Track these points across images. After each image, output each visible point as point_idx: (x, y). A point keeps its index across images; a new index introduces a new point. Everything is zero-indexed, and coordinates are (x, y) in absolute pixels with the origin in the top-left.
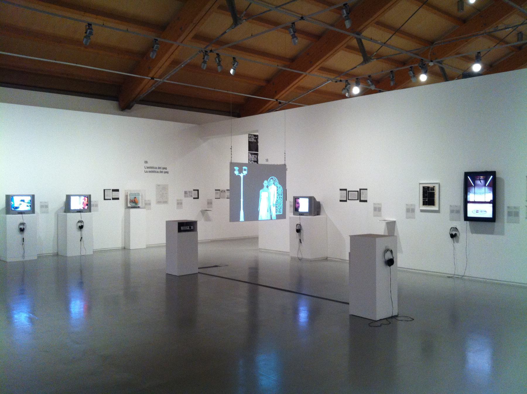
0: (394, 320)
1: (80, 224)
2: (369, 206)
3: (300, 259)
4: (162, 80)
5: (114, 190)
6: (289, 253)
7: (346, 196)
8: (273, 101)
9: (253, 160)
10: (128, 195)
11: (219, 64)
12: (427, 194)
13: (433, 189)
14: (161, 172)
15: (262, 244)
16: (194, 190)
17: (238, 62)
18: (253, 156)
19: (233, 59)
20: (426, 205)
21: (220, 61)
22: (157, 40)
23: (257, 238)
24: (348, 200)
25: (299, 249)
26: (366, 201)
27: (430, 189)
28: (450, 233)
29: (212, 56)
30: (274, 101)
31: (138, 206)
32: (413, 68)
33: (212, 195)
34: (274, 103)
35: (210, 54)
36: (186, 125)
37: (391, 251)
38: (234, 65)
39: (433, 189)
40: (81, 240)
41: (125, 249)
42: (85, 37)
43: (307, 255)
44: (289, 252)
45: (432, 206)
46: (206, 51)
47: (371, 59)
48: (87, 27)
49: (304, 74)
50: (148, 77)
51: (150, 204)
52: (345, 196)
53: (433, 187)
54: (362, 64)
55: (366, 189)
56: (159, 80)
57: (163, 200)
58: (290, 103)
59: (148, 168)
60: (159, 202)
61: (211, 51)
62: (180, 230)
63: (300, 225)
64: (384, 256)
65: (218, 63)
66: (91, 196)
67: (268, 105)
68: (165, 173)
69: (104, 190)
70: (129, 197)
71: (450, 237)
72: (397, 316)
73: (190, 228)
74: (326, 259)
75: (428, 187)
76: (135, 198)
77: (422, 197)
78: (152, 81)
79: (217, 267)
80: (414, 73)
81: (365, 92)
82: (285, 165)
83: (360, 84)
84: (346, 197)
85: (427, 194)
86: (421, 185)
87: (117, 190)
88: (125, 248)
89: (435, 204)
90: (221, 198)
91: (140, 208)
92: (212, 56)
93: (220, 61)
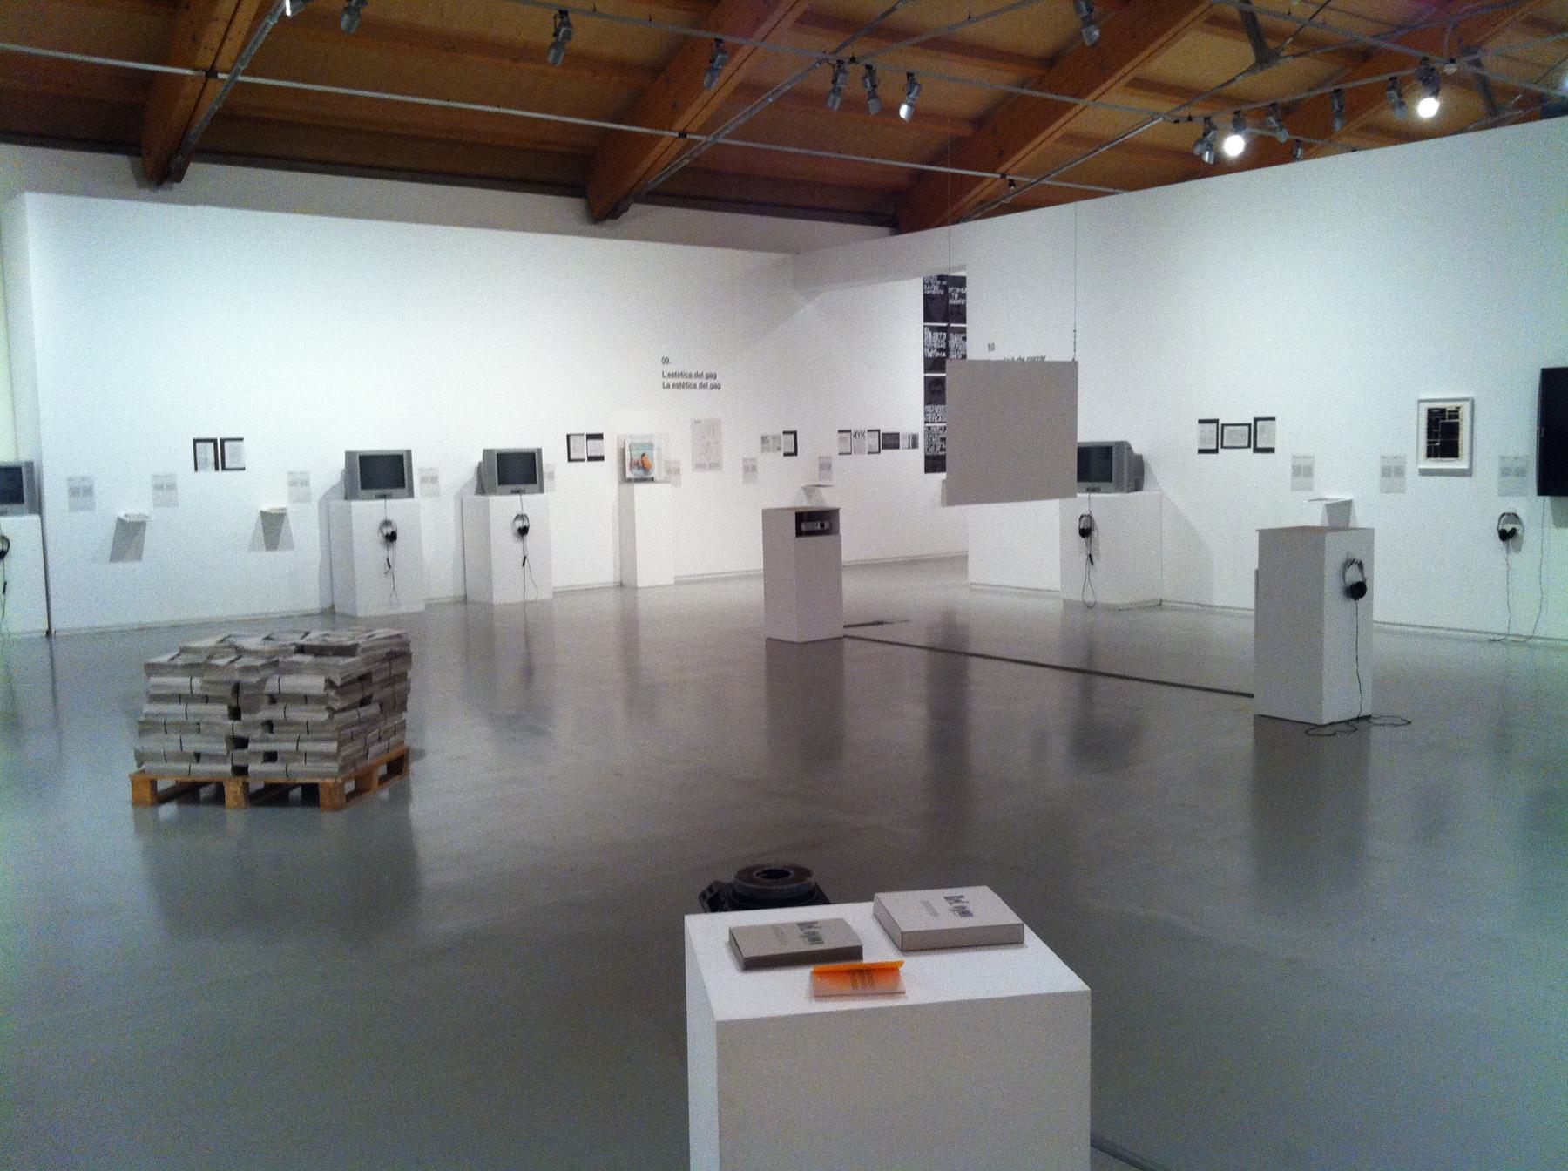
0: (1362, 724)
1: (519, 524)
2: (1278, 464)
3: (1090, 607)
4: (710, 138)
5: (590, 437)
6: (1058, 592)
7: (1215, 438)
8: (992, 178)
9: (935, 345)
10: (627, 448)
11: (873, 95)
12: (1438, 428)
13: (1455, 414)
14: (703, 386)
15: (978, 572)
16: (784, 433)
17: (919, 85)
18: (937, 334)
19: (908, 78)
20: (1436, 456)
21: (874, 86)
22: (721, 41)
23: (966, 557)
24: (1220, 449)
25: (1087, 579)
26: (1271, 450)
27: (1447, 413)
28: (1498, 528)
29: (856, 71)
30: (996, 179)
31: (651, 476)
32: (1398, 81)
33: (830, 444)
34: (996, 184)
35: (849, 67)
36: (775, 256)
37: (1360, 565)
38: (909, 93)
39: (1455, 414)
40: (524, 564)
41: (624, 586)
42: (554, 45)
43: (1109, 592)
44: (1059, 589)
45: (1453, 459)
46: (840, 62)
47: (1278, 55)
48: (559, 20)
49: (1082, 103)
50: (670, 130)
51: (677, 471)
52: (1213, 439)
53: (1454, 409)
54: (1251, 70)
55: (1273, 419)
56: (703, 138)
57: (708, 461)
58: (1045, 181)
59: (671, 375)
60: (699, 466)
61: (853, 60)
62: (799, 533)
63: (1090, 517)
64: (1344, 576)
65: (869, 92)
66: (543, 452)
67: (977, 190)
68: (712, 388)
69: (568, 436)
70: (627, 454)
71: (1498, 536)
72: (1368, 718)
73: (822, 525)
74: (1159, 605)
75: (1443, 411)
76: (643, 455)
77: (1426, 435)
78: (682, 140)
79: (879, 626)
80: (1400, 95)
81: (1262, 156)
82: (1074, 364)
83: (1244, 129)
84: (1215, 442)
85: (1440, 427)
86: (1422, 404)
87: (599, 436)
88: (621, 585)
89: (1460, 452)
90: (855, 453)
91: (657, 482)
92: (856, 71)
93: (874, 86)
